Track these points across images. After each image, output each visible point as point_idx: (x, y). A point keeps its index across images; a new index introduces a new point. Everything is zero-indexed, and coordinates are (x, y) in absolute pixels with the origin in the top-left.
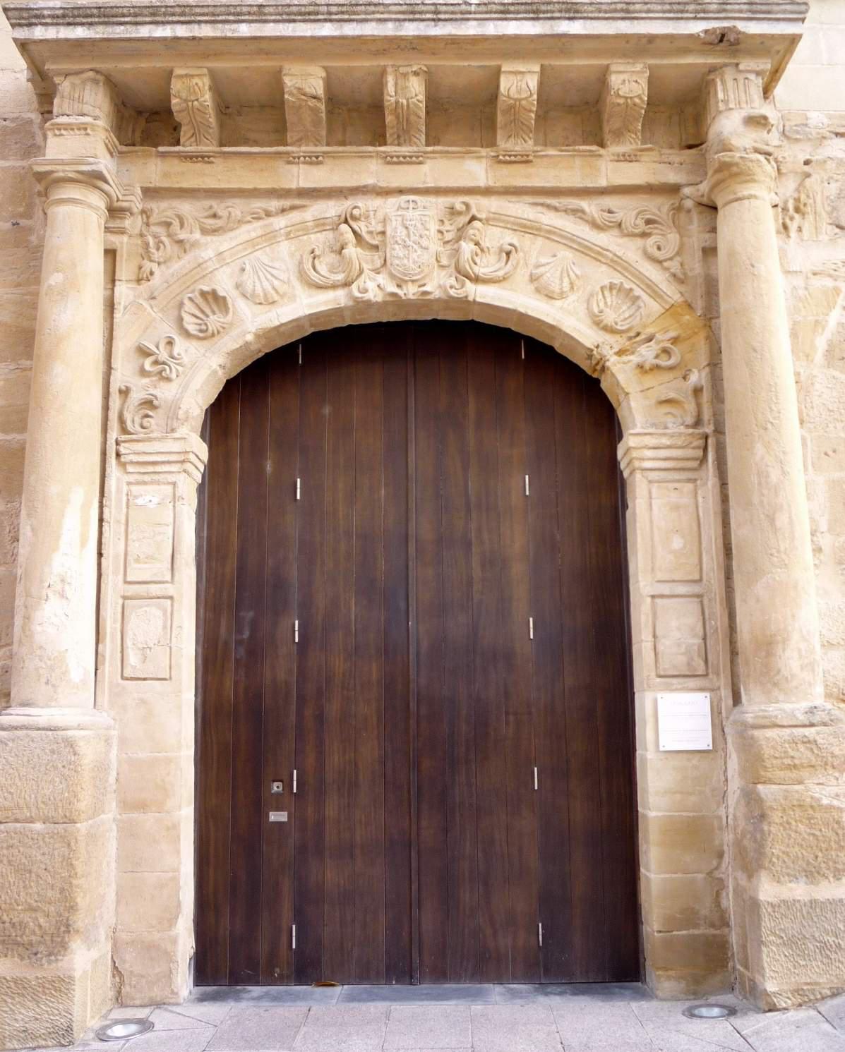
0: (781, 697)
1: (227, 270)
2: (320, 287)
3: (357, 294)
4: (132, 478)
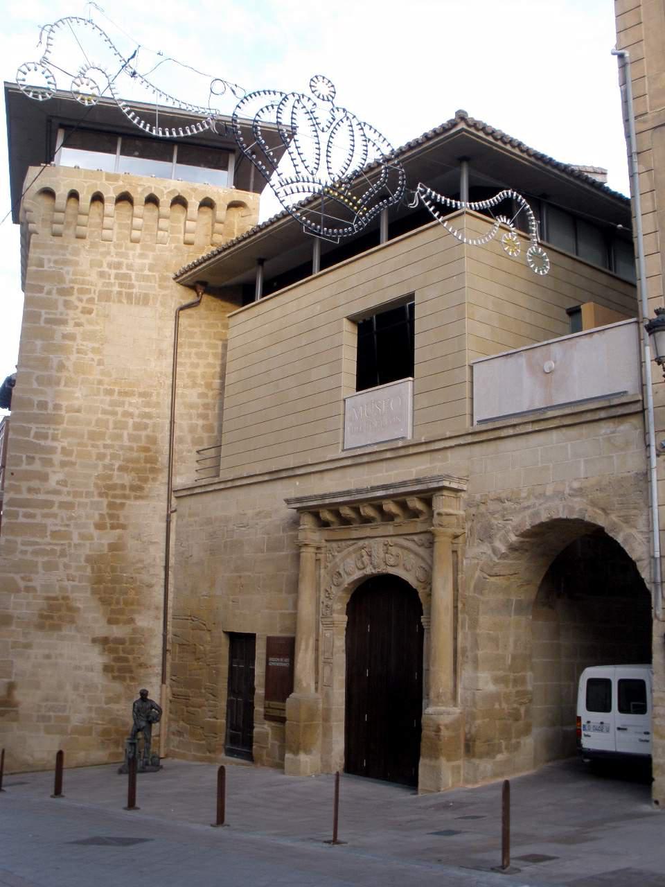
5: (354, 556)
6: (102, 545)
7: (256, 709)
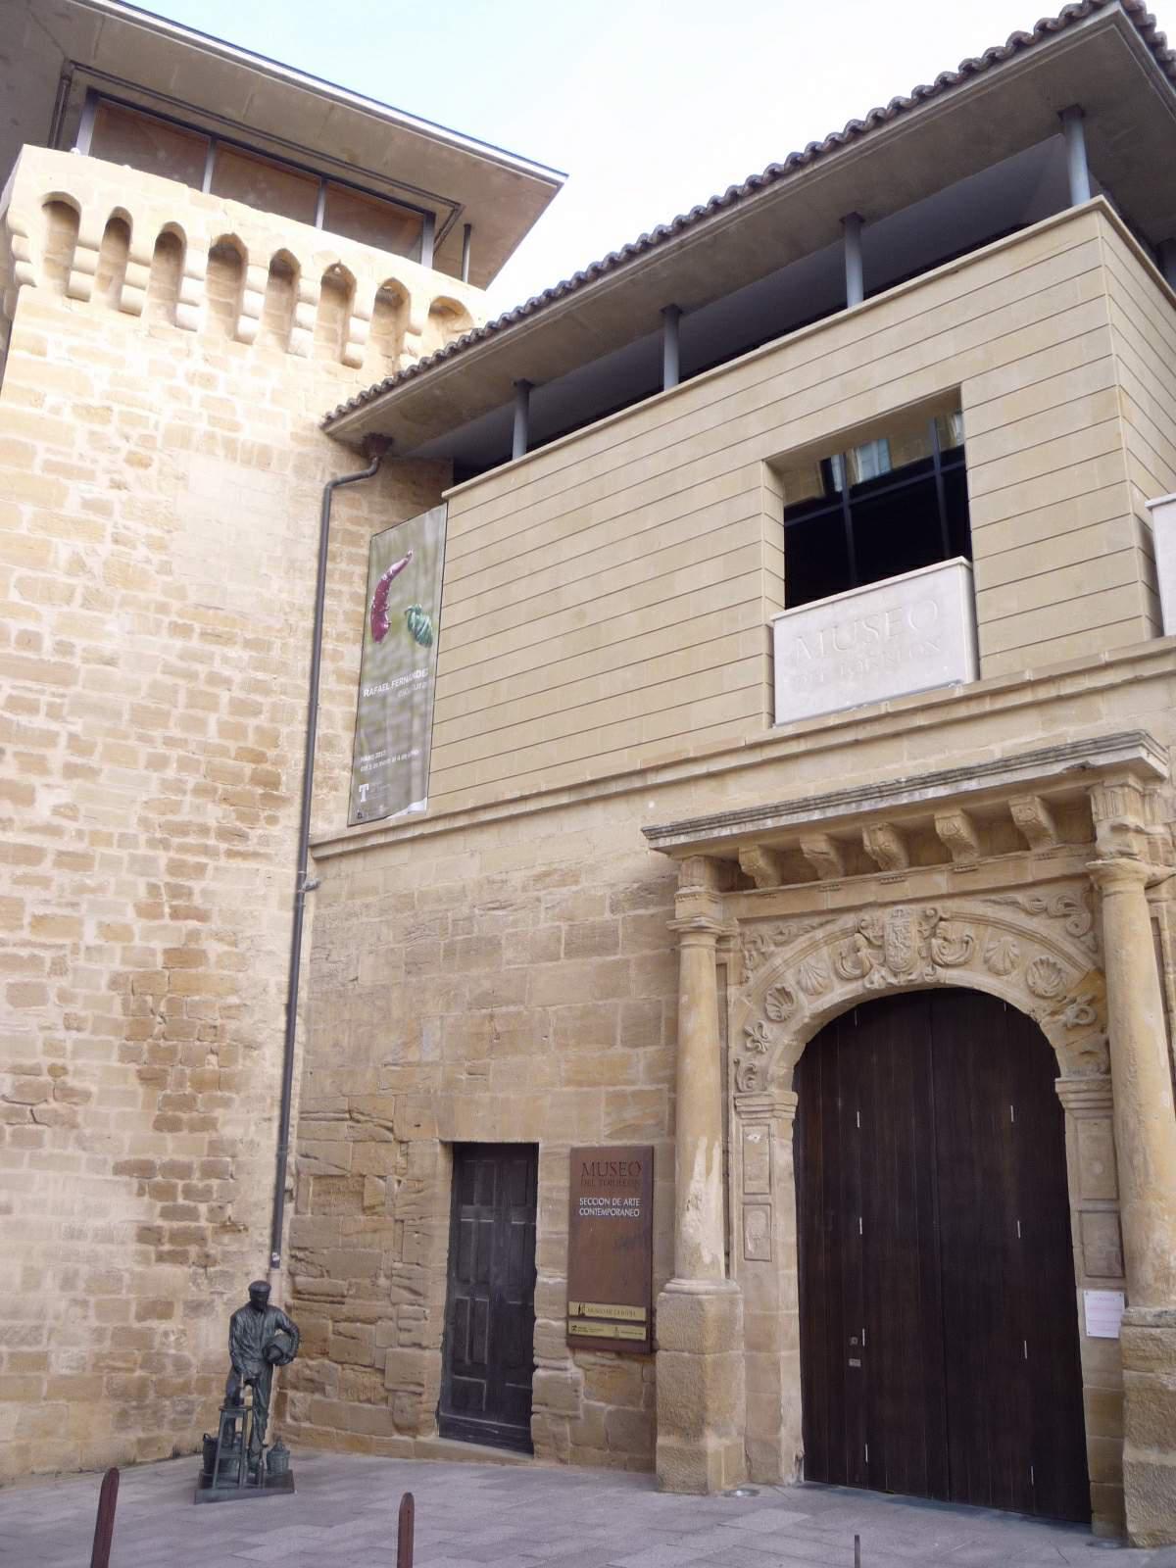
0: (1141, 1302)
1: (792, 970)
2: (848, 980)
3: (868, 986)
4: (745, 1122)
5: (825, 951)
6: (152, 952)
7: (539, 1321)
